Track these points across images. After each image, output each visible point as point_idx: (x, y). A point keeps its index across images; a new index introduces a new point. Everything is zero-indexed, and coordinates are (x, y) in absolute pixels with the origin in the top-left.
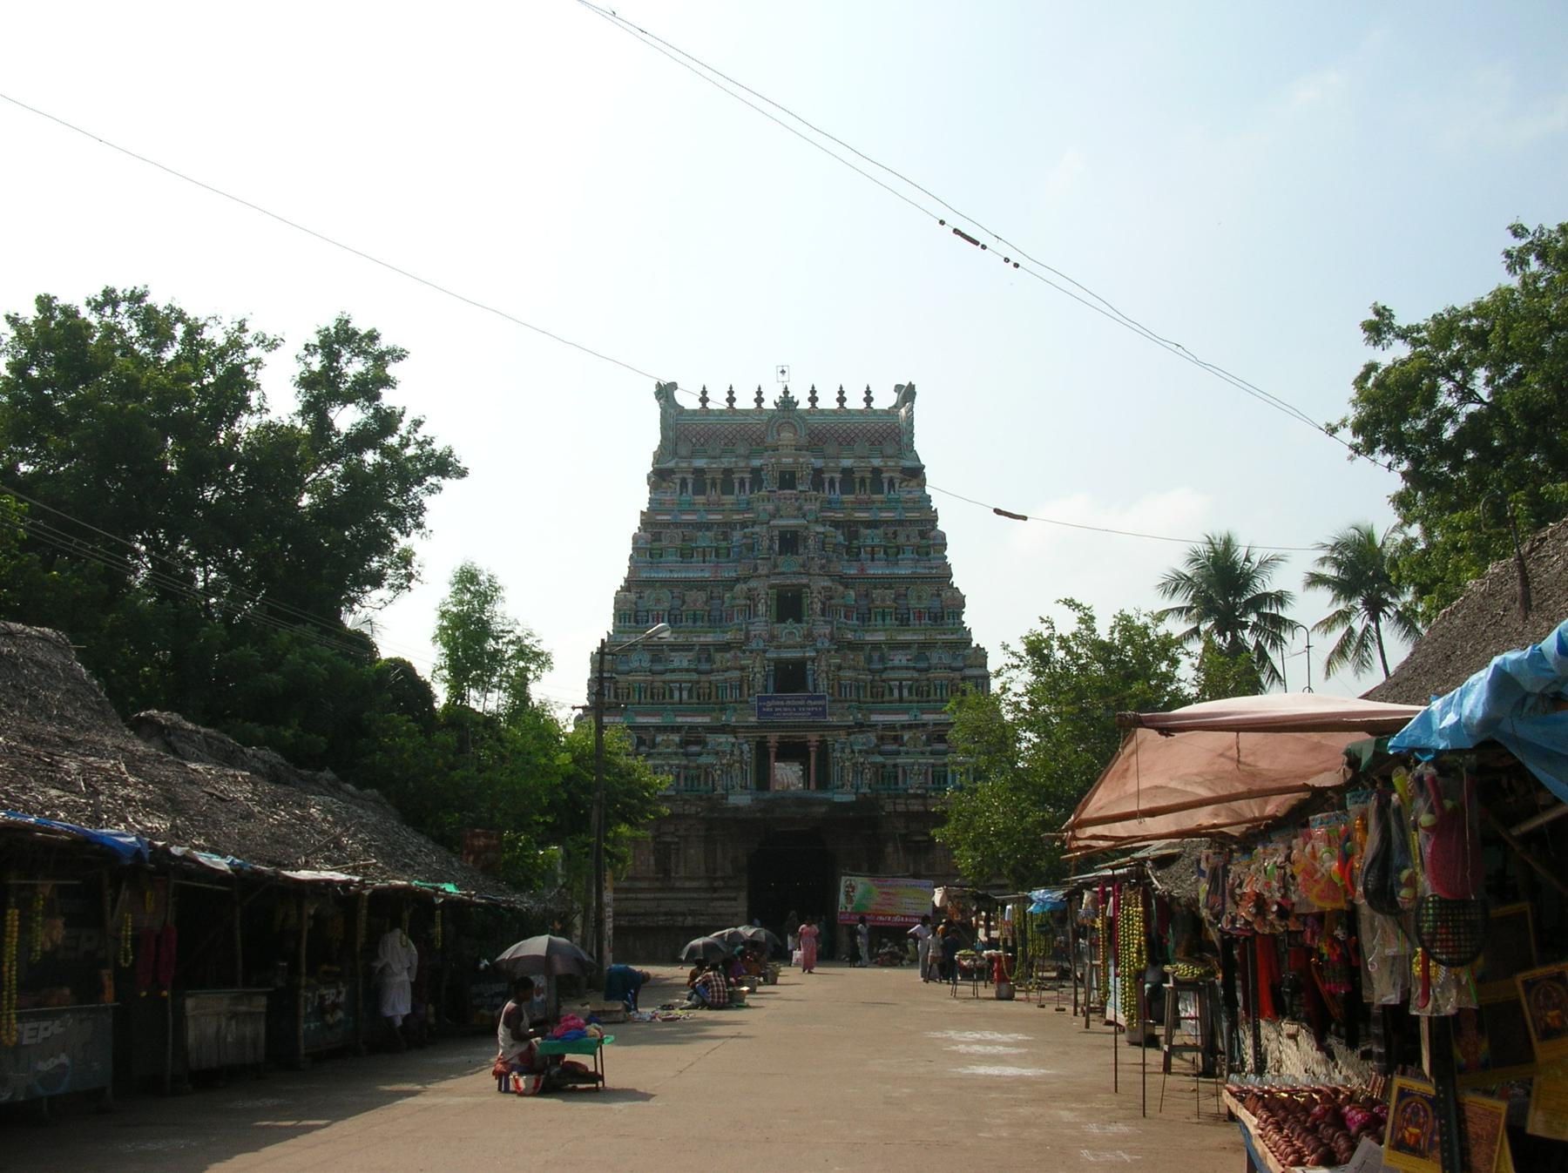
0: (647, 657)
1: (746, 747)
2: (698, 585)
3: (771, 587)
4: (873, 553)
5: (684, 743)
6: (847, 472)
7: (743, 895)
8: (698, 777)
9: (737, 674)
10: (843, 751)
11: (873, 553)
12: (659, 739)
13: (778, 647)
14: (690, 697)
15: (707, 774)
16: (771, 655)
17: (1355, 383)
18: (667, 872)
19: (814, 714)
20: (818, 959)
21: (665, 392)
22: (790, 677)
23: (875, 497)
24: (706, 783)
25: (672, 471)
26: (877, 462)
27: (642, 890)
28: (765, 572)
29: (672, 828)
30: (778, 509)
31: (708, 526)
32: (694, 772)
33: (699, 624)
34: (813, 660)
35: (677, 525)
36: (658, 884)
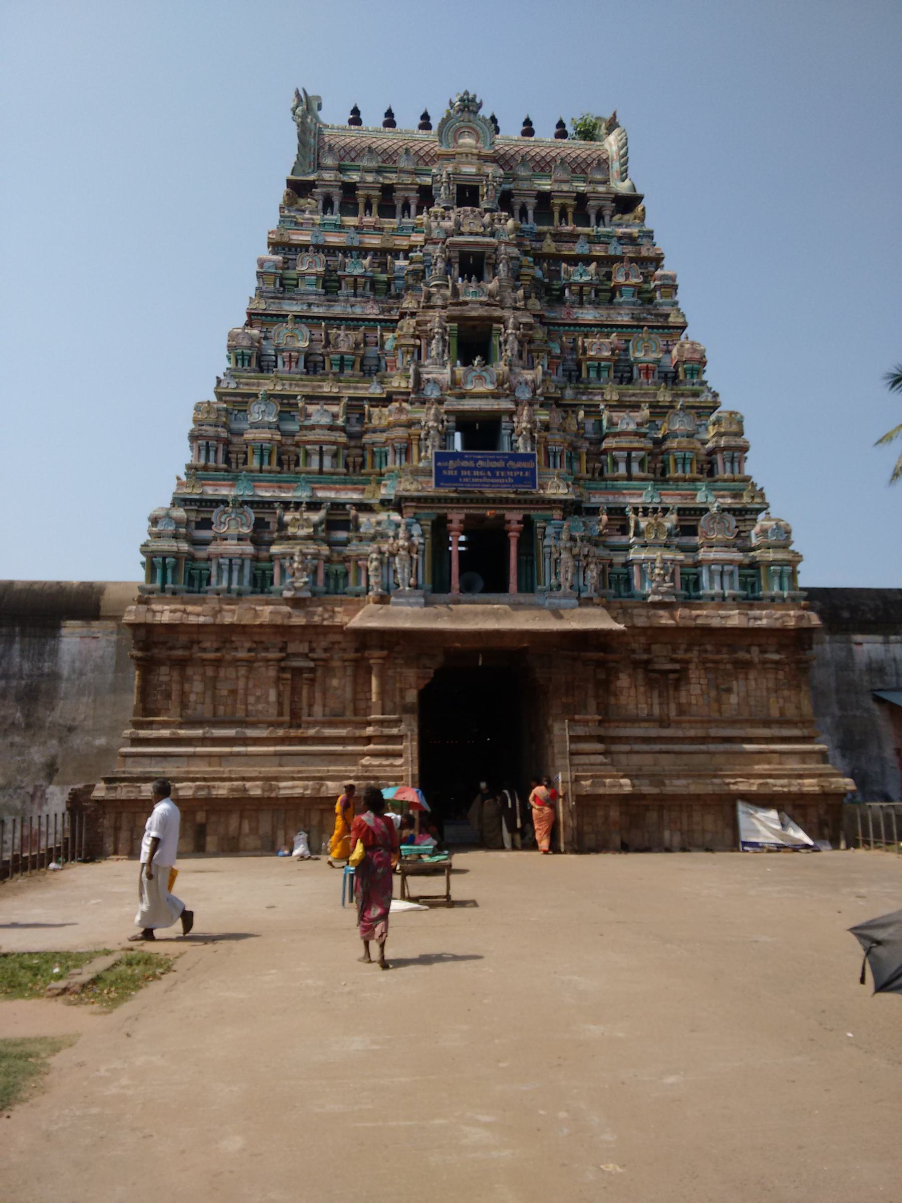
0: (275, 407)
1: (416, 530)
2: (352, 323)
3: (451, 319)
4: (581, 294)
5: (331, 525)
6: (544, 198)
7: (410, 747)
8: (346, 574)
9: (400, 432)
10: (558, 537)
11: (581, 294)
12: (288, 517)
13: (462, 396)
14: (335, 465)
15: (358, 568)
16: (452, 404)
17: (191, 914)
18: (295, 714)
19: (519, 480)
20: (178, 858)
21: (306, 108)
22: (481, 431)
23: (580, 229)
24: (358, 583)
25: (312, 185)
26: (582, 187)
27: (256, 741)
28: (440, 302)
29: (304, 648)
30: (458, 224)
31: (363, 252)
32: (340, 568)
33: (348, 371)
34: (511, 414)
35: (320, 248)
36: (281, 732)
